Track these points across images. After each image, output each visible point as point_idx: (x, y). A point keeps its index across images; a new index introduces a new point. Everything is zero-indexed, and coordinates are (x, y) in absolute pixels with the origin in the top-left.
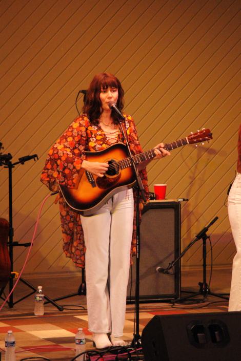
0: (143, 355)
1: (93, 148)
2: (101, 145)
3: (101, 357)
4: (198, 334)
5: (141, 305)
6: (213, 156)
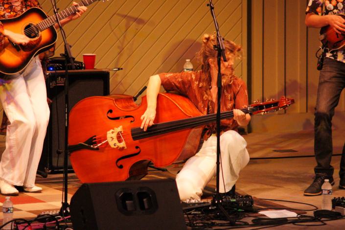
0: (71, 224)
1: (285, 91)
2: (10, 12)
3: (29, 225)
4: (127, 202)
5: (69, 175)
6: (141, 26)
